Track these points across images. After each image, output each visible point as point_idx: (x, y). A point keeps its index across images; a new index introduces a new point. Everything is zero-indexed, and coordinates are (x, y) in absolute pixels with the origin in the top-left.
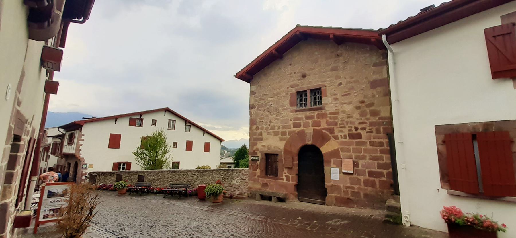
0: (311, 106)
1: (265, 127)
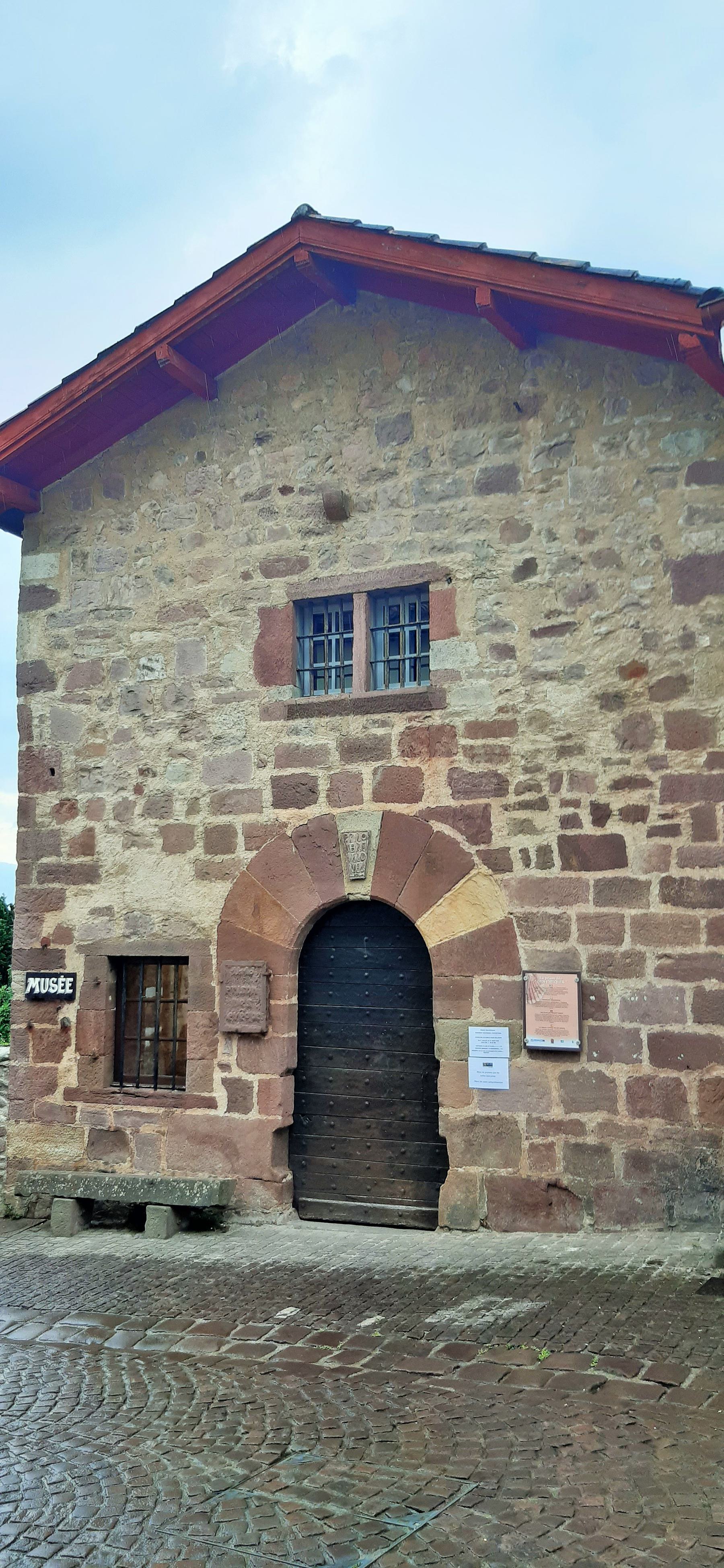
0: (371, 682)
1: (110, 798)
